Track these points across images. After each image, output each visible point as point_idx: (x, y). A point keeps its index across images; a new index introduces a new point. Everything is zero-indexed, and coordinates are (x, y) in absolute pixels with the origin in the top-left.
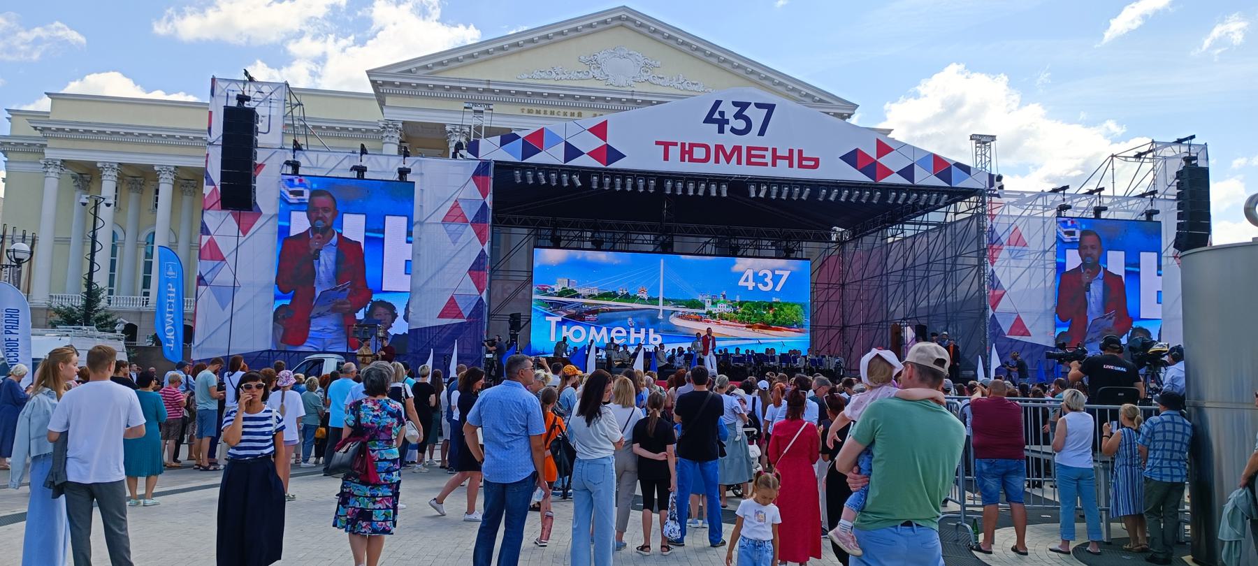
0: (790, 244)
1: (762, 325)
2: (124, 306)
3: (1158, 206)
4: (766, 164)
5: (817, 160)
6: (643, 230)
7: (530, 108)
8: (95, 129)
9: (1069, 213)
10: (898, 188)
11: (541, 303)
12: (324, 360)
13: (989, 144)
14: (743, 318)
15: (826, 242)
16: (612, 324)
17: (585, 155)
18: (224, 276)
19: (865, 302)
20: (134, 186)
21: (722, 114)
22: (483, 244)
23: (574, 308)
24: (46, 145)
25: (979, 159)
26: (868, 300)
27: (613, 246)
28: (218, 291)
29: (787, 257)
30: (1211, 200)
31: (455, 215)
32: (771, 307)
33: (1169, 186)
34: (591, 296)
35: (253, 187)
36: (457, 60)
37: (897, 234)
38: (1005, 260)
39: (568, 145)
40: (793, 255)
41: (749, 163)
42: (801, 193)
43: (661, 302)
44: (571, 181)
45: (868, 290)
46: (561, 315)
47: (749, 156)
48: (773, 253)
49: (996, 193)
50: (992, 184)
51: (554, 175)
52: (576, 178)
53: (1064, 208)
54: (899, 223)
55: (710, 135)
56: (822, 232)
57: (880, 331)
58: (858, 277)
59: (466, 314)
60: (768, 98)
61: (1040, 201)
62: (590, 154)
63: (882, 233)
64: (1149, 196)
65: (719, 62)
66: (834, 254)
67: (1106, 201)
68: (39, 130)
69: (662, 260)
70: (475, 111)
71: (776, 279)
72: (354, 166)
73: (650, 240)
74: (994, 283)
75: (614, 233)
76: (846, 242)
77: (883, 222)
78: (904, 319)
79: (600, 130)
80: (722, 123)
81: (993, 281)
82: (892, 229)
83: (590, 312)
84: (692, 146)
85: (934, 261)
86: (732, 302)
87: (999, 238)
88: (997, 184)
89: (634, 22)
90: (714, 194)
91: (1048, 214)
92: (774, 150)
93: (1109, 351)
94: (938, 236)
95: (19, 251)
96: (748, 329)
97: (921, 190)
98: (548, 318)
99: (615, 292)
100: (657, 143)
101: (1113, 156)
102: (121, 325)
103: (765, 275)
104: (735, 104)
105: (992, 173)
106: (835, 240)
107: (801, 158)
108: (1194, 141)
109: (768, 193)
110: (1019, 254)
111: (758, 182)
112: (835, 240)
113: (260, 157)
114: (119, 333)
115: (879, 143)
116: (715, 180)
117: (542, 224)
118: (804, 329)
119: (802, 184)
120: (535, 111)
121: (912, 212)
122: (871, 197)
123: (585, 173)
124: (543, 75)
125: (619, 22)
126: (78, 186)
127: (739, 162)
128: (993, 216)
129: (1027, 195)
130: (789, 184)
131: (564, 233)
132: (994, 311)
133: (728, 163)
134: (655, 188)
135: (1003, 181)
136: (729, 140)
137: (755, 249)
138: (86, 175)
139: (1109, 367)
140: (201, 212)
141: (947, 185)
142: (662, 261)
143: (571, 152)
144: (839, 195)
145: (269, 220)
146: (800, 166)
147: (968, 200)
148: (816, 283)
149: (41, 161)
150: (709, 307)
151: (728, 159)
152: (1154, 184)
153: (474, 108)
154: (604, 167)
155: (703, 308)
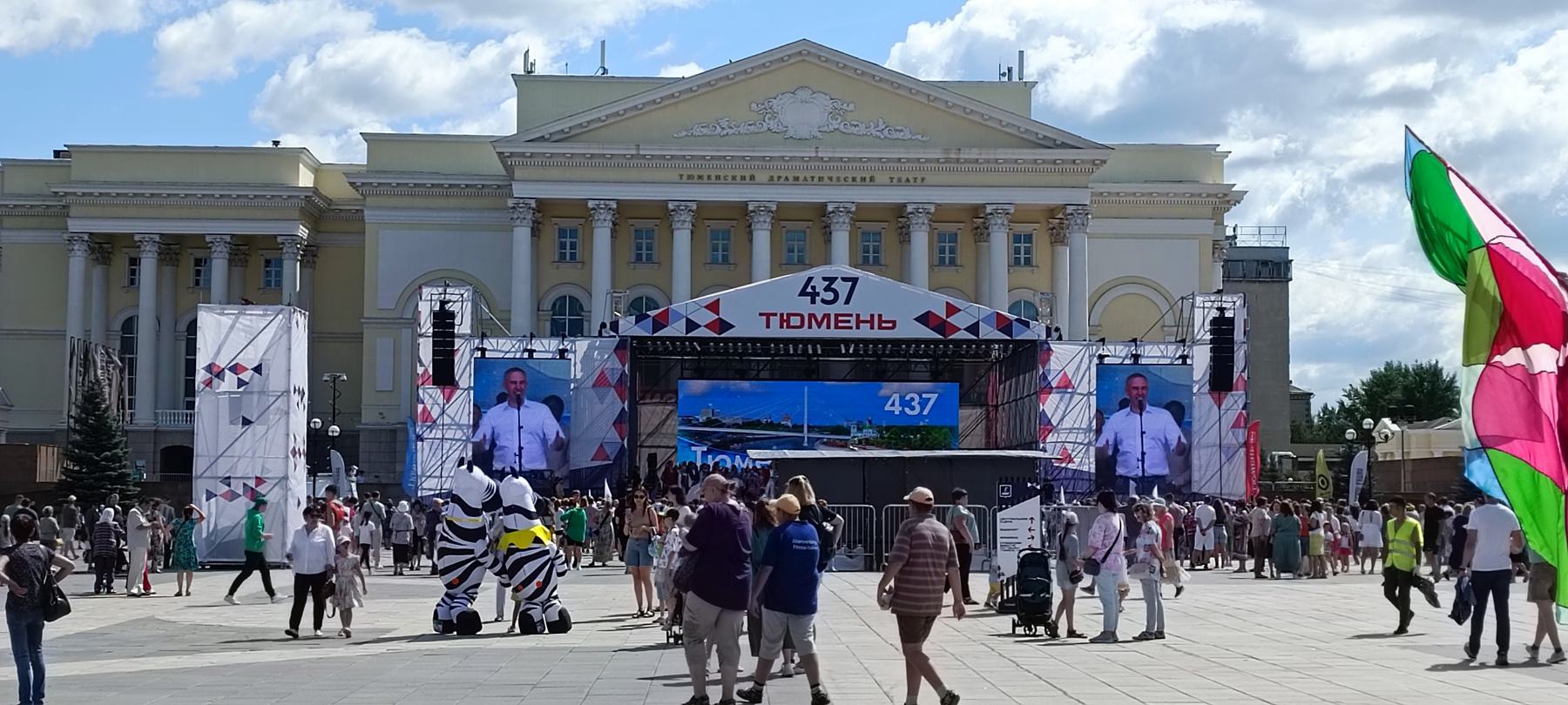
4: (851, 328)
5: (894, 323)
7: (690, 173)
21: (814, 288)
27: (758, 375)
30: (239, 589)
31: (601, 382)
39: (688, 320)
41: (837, 327)
43: (806, 429)
46: (706, 445)
47: (837, 321)
55: (804, 306)
59: (612, 457)
79: (714, 307)
80: (814, 295)
83: (734, 441)
84: (789, 315)
92: (858, 316)
98: (693, 448)
99: (759, 421)
100: (761, 314)
103: (913, 399)
104: (825, 279)
119: (884, 342)
120: (696, 177)
123: (703, 341)
124: (705, 131)
125: (800, 58)
127: (828, 327)
133: (819, 327)
136: (820, 309)
143: (691, 325)
146: (880, 327)
151: (819, 325)
154: (717, 336)
155: (849, 434)
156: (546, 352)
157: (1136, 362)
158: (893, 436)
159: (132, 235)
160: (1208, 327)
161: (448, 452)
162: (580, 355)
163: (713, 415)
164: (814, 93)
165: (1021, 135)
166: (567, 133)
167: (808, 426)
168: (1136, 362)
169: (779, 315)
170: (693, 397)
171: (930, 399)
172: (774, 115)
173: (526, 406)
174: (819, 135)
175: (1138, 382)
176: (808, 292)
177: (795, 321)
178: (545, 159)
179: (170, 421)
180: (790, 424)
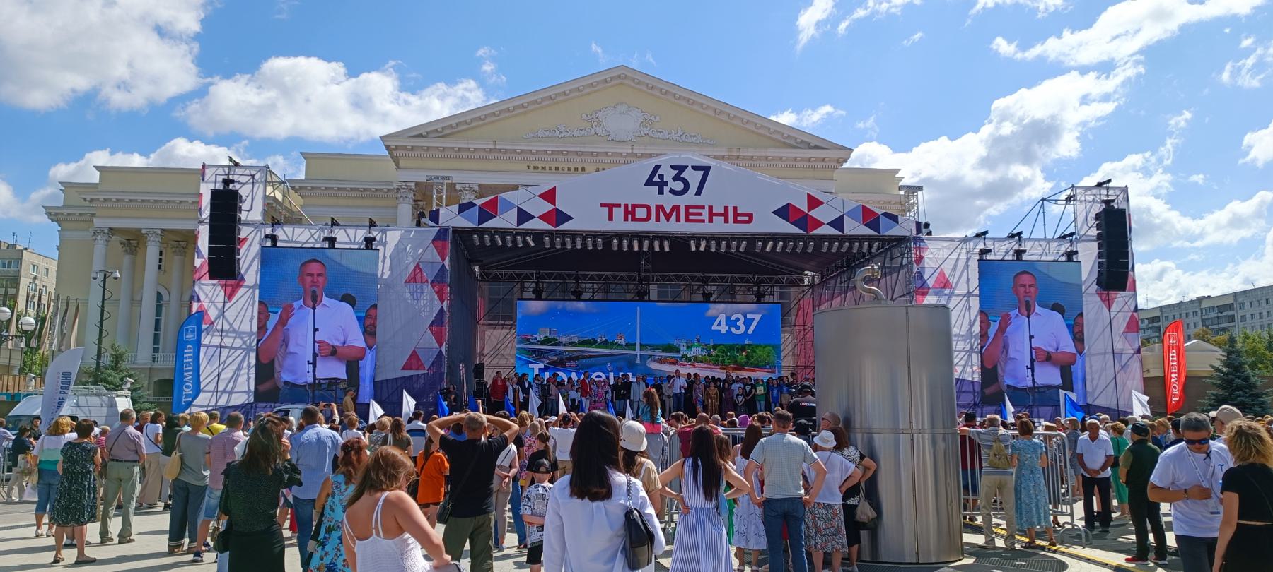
1: (735, 366)
4: (703, 221)
5: (751, 216)
9: (990, 257)
10: (831, 239)
11: (524, 352)
12: (289, 411)
14: (717, 361)
20: (177, 249)
21: (661, 177)
22: (442, 302)
23: (556, 356)
29: (758, 302)
31: (415, 277)
32: (743, 348)
33: (1090, 227)
34: (572, 344)
35: (236, 260)
41: (687, 220)
44: (525, 242)
46: (543, 362)
47: (687, 214)
51: (509, 237)
55: (651, 196)
56: (794, 276)
62: (541, 217)
65: (716, 114)
71: (748, 323)
79: (550, 196)
80: (661, 185)
83: (570, 359)
84: (634, 206)
86: (706, 345)
88: (924, 230)
90: (657, 249)
92: (711, 208)
95: (26, 324)
96: (722, 371)
98: (531, 366)
99: (594, 339)
100: (603, 205)
101: (1043, 200)
103: (738, 319)
104: (673, 167)
107: (736, 214)
108: (1110, 185)
109: (708, 247)
111: (698, 237)
113: (244, 232)
117: (527, 277)
119: (739, 238)
120: (540, 168)
123: (538, 235)
124: (547, 134)
125: (619, 81)
126: (126, 251)
127: (678, 220)
135: (931, 228)
136: (668, 201)
138: (133, 242)
143: (524, 216)
144: (775, 246)
146: (735, 221)
150: (684, 350)
151: (668, 217)
154: (553, 228)
156: (351, 243)
157: (1019, 259)
158: (719, 354)
159: (140, 230)
160: (1091, 222)
161: (225, 362)
162: (390, 248)
163: (550, 334)
164: (629, 107)
165: (784, 140)
166: (441, 132)
167: (641, 344)
168: (1019, 259)
169: (623, 206)
171: (754, 319)
172: (600, 123)
173: (324, 305)
174: (634, 139)
175: (1026, 279)
177: (641, 213)
178: (423, 152)
179: (164, 361)
180: (623, 342)
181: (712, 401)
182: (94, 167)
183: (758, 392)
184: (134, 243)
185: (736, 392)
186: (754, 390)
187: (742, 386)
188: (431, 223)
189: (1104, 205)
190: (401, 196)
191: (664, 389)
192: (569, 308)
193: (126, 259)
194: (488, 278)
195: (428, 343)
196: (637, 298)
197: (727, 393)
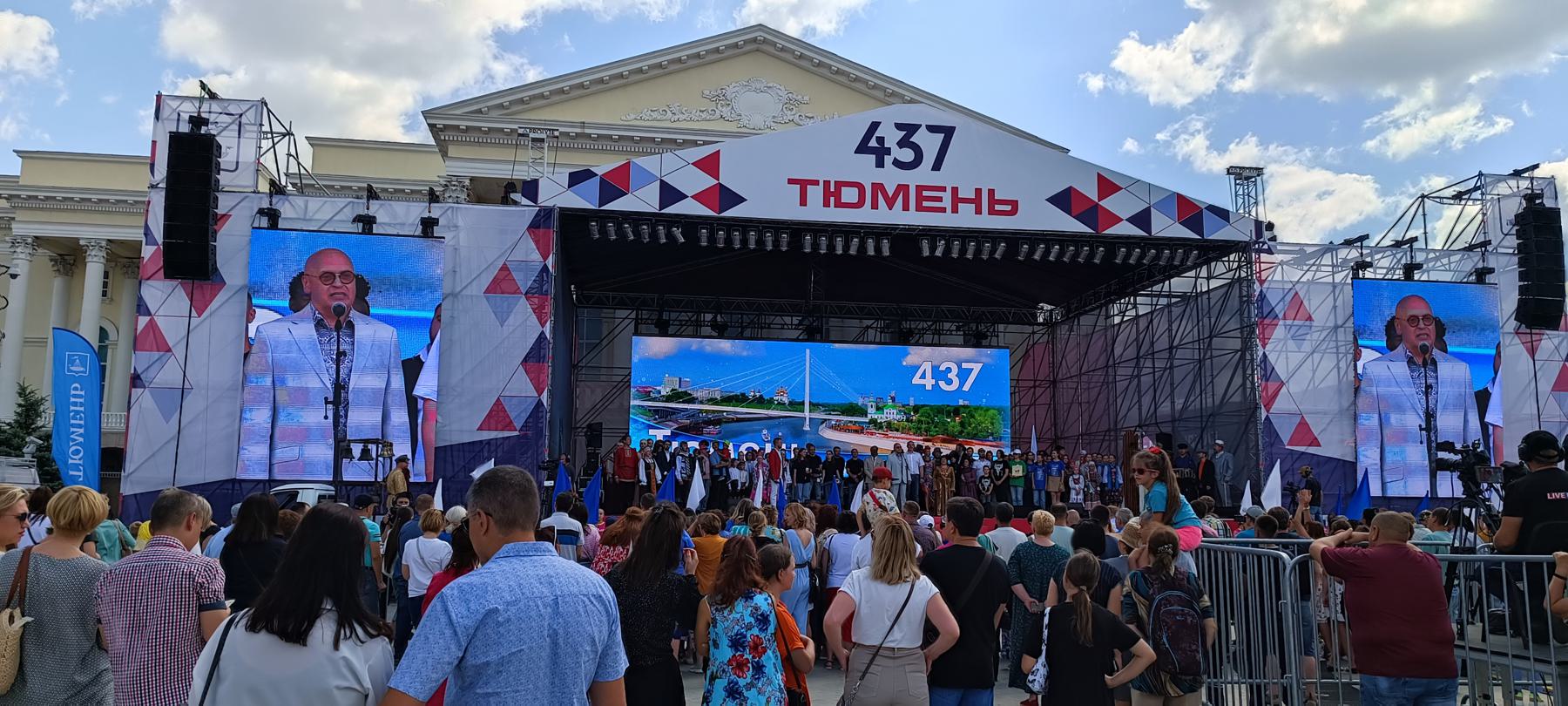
0: (982, 327)
1: (945, 437)
2: (114, 425)
3: (1492, 262)
4: (943, 210)
5: (1014, 204)
6: (782, 312)
8: (77, 196)
9: (1369, 274)
10: (1128, 241)
12: (298, 492)
13: (1253, 179)
15: (1030, 325)
16: (743, 437)
17: (689, 198)
18: (168, 374)
19: (1084, 407)
21: (881, 140)
22: (543, 325)
24: (13, 219)
25: (1240, 201)
26: (1088, 402)
27: (742, 333)
28: (161, 393)
29: (977, 345)
31: (502, 284)
32: (956, 411)
33: (1506, 235)
36: (542, 96)
37: (1126, 310)
38: (1280, 340)
39: (664, 185)
40: (984, 342)
41: (919, 208)
42: (993, 251)
44: (669, 235)
45: (1089, 388)
47: (920, 198)
48: (961, 340)
49: (1266, 247)
50: (1259, 234)
52: (677, 232)
53: (1362, 265)
54: (1129, 295)
57: (1105, 444)
58: (1074, 371)
59: (518, 424)
60: (945, 119)
61: (1327, 259)
62: (696, 197)
63: (1107, 310)
64: (1479, 250)
66: (1041, 341)
67: (1420, 258)
68: (5, 198)
69: (808, 351)
70: (534, 140)
71: (964, 374)
72: (357, 216)
73: (792, 325)
74: (1268, 372)
75: (742, 314)
76: (1057, 323)
77: (1108, 294)
78: (1139, 426)
80: (881, 153)
81: (1265, 370)
82: (1120, 303)
83: (709, 423)
84: (839, 185)
85: (1179, 345)
86: (903, 406)
87: (1273, 309)
88: (1267, 234)
89: (774, 44)
90: (871, 252)
91: (1339, 277)
93: (1539, 462)
94: (1185, 311)
97: (1161, 244)
100: (791, 181)
101: (1423, 197)
102: (32, 446)
104: (899, 126)
105: (1260, 220)
106: (1042, 321)
108: (1537, 173)
109: (948, 250)
110: (1300, 332)
111: (933, 234)
112: (1042, 321)
113: (224, 204)
114: (28, 457)
115: (1101, 179)
116: (873, 234)
118: (1002, 442)
121: (1148, 279)
122: (1092, 254)
123: (690, 224)
124: (655, 115)
126: (58, 270)
128: (1262, 282)
129: (1309, 250)
130: (976, 237)
131: (673, 316)
132: (1268, 411)
134: (789, 244)
135: (1276, 232)
136: (891, 177)
137: (933, 334)
138: (68, 257)
139: (1556, 495)
140: (138, 283)
141: (1199, 237)
142: (808, 351)
143: (670, 194)
144: (1047, 252)
145: (235, 294)
146: (992, 212)
147: (1226, 259)
148: (1018, 380)
149: (7, 239)
150: (872, 413)
151: (890, 203)
152: (1484, 227)
153: (532, 135)
154: (711, 213)
158: (923, 419)
163: (680, 387)
169: (821, 184)
170: (652, 363)
176: (870, 145)
177: (850, 195)
181: (943, 486)
182: (14, 151)
183: (1014, 474)
184: (70, 259)
185: (981, 473)
186: (1007, 470)
187: (989, 464)
188: (525, 201)
189: (1524, 202)
190: (450, 197)
191: (866, 468)
192: (708, 349)
193: (57, 283)
194: (588, 303)
195: (522, 390)
196: (806, 337)
197: (969, 474)
